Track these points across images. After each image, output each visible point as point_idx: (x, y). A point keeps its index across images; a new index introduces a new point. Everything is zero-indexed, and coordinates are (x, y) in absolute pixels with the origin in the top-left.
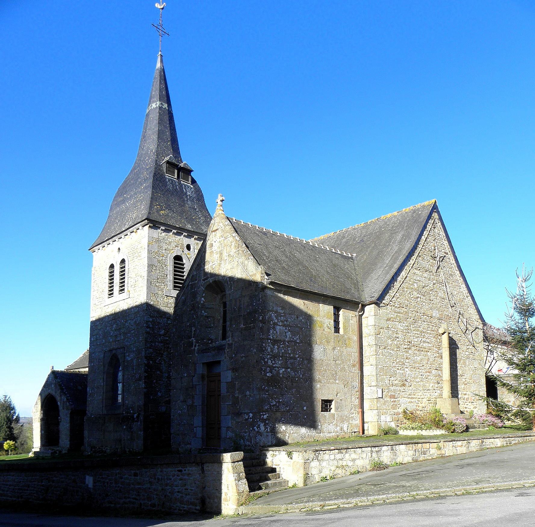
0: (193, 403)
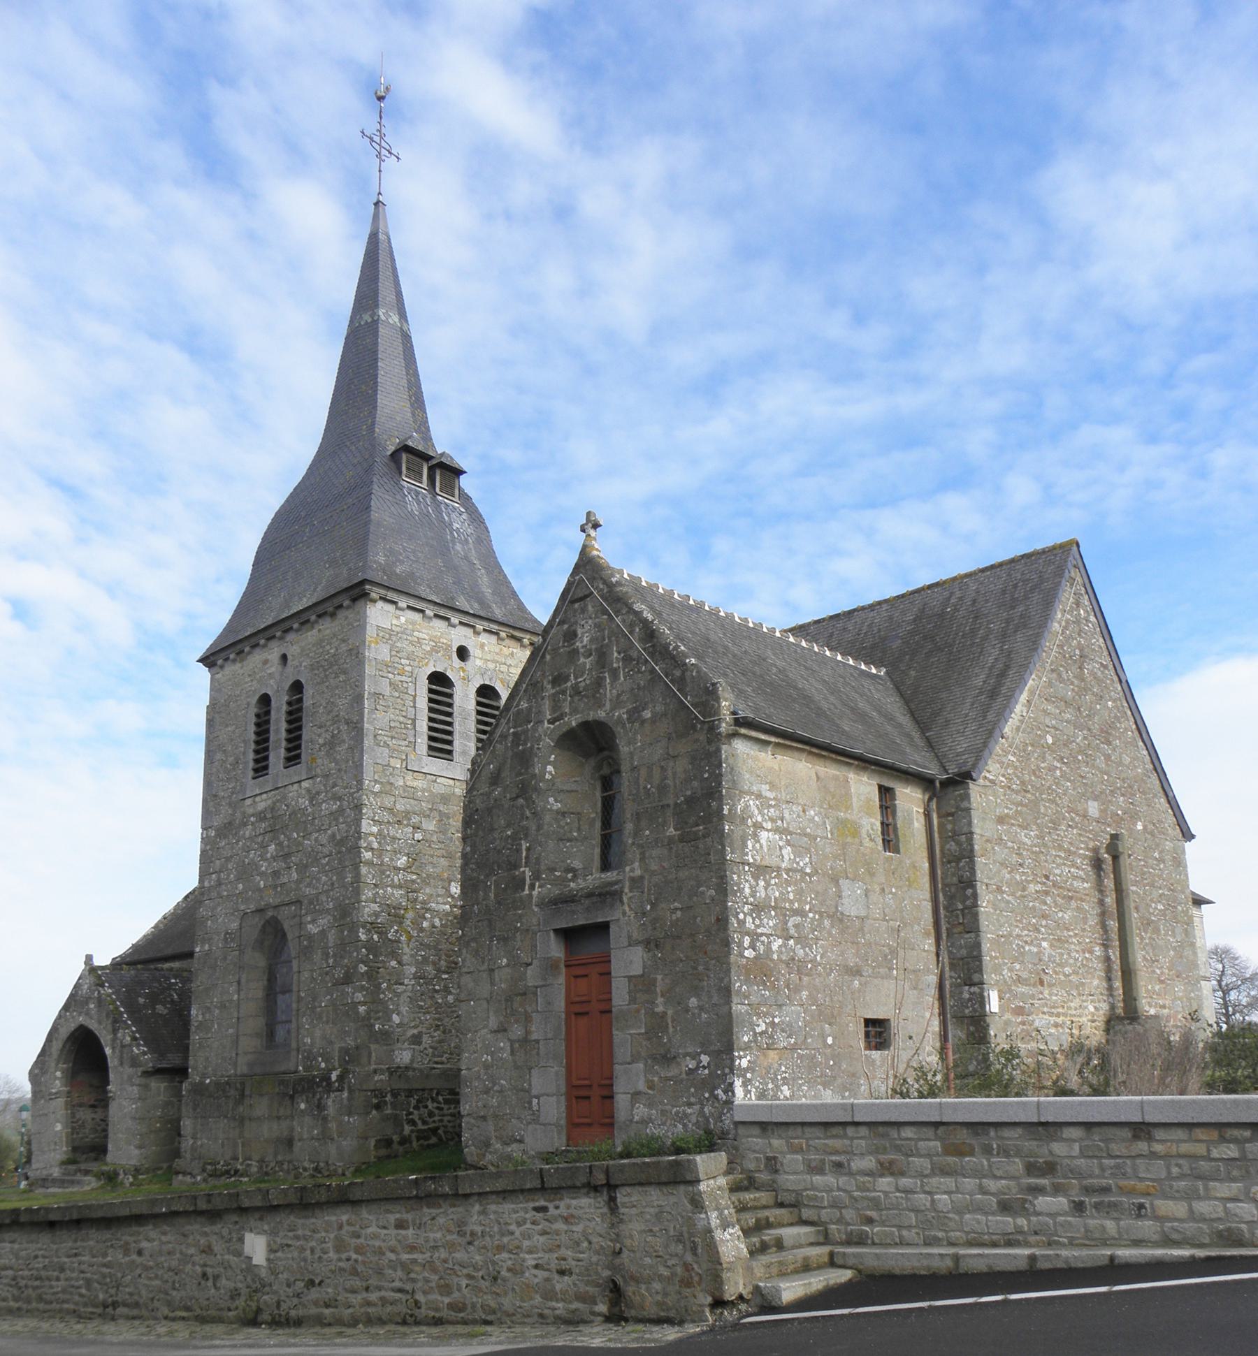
0: (528, 1033)
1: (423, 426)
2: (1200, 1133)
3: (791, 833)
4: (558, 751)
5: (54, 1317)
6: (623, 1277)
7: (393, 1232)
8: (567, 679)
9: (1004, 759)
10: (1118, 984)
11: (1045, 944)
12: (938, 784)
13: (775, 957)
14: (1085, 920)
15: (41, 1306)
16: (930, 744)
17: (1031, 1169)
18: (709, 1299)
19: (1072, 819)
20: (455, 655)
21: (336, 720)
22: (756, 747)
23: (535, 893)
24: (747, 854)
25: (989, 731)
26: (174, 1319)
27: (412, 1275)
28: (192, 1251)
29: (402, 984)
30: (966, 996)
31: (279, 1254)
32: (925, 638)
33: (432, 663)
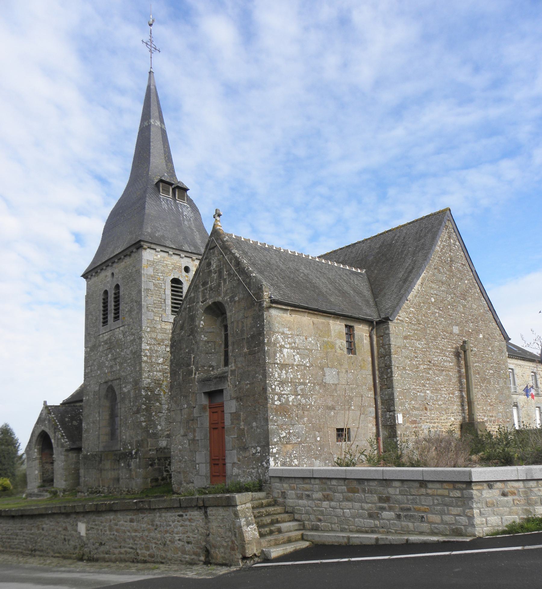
0: (195, 436)
1: (171, 171)
2: (445, 486)
3: (299, 349)
4: (205, 315)
5: (14, 555)
6: (210, 545)
7: (129, 523)
8: (207, 283)
9: (408, 310)
10: (466, 407)
11: (428, 392)
12: (375, 323)
13: (291, 404)
14: (450, 380)
15: (11, 550)
16: (376, 304)
17: (381, 499)
18: (241, 556)
19: (444, 335)
20: (183, 270)
21: (132, 301)
22: (281, 312)
23: (196, 377)
24: (277, 359)
25: (401, 297)
26: (55, 557)
27: (136, 542)
28: (60, 529)
29: (162, 413)
30: (388, 416)
31: (90, 532)
32: (383, 255)
33: (172, 274)
